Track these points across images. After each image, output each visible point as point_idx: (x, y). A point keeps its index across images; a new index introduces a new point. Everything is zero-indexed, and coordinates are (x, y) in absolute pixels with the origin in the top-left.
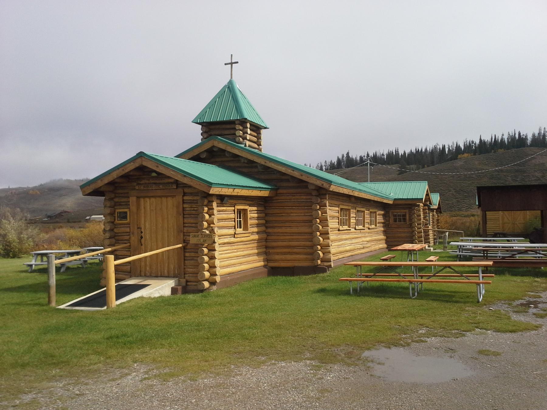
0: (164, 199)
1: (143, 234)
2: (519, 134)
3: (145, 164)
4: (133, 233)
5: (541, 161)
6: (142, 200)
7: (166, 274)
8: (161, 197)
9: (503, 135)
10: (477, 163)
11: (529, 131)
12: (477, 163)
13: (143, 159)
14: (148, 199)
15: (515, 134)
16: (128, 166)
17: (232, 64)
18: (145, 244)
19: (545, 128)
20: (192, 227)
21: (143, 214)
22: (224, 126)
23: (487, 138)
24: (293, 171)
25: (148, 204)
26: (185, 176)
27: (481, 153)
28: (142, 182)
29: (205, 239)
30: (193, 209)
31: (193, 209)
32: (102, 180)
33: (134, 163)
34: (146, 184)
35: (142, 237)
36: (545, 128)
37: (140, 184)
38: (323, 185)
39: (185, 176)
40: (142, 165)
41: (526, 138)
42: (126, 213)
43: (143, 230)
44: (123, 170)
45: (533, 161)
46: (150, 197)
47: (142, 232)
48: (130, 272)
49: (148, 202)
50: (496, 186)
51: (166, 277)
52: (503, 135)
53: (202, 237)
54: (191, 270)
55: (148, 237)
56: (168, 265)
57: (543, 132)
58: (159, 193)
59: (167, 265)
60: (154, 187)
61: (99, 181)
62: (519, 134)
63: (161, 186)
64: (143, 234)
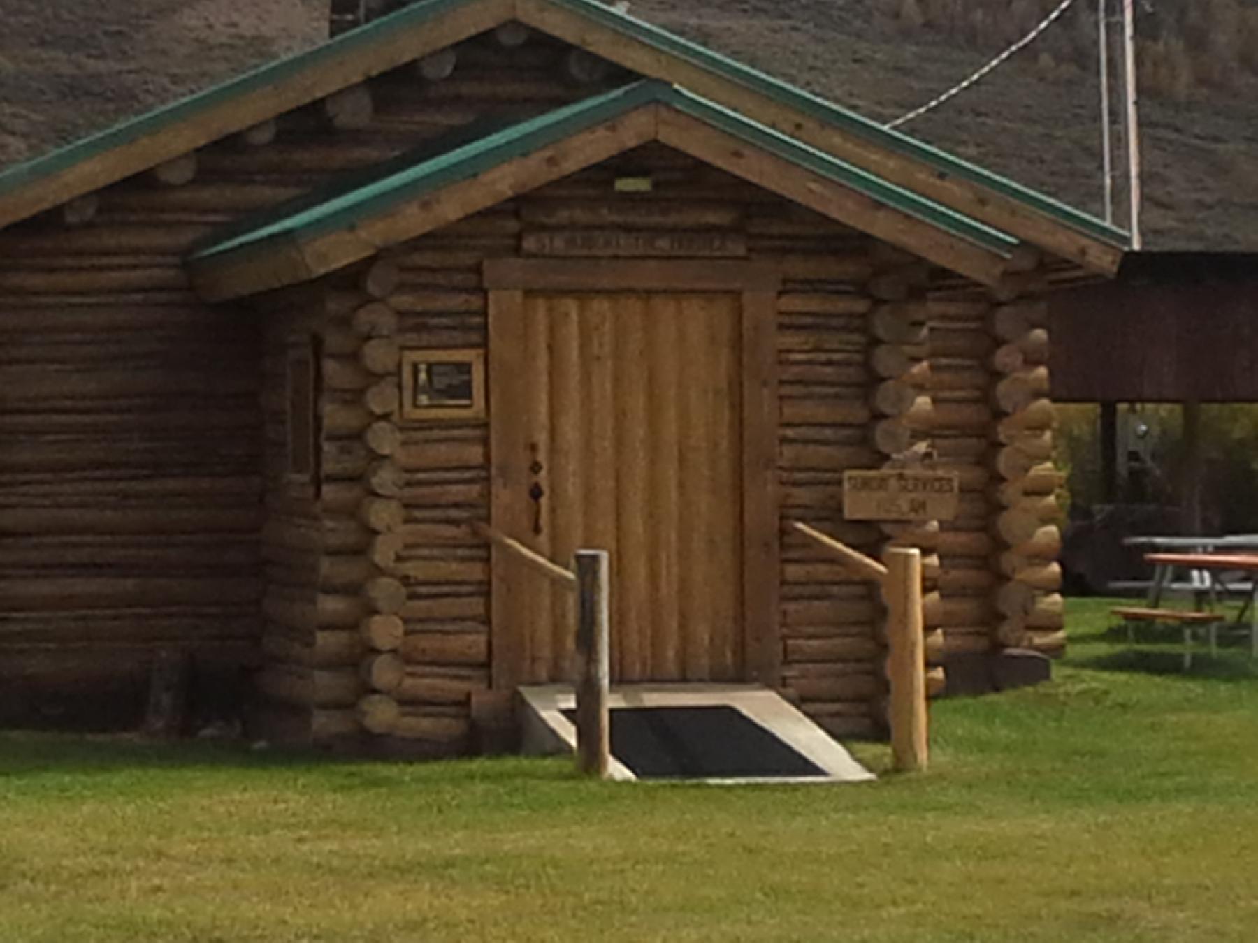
0: (666, 309)
1: (543, 477)
3: (671, 136)
4: (503, 471)
5: (247, 26)
6: (541, 305)
7: (672, 668)
13: (664, 113)
14: (571, 306)
16: (577, 141)
18: (553, 526)
20: (825, 443)
21: (544, 379)
24: (942, 176)
25: (573, 329)
26: (880, 206)
28: (552, 221)
29: (918, 496)
30: (823, 357)
31: (823, 357)
32: (425, 206)
33: (613, 128)
34: (572, 226)
35: (536, 493)
37: (543, 228)
38: (1083, 252)
39: (880, 206)
40: (656, 141)
42: (465, 368)
43: (542, 457)
46: (583, 294)
48: (487, 665)
49: (574, 316)
50: (1171, 255)
51: (672, 681)
53: (904, 489)
54: (814, 643)
55: (572, 489)
56: (682, 626)
58: (650, 275)
59: (674, 624)
60: (625, 245)
61: (413, 210)
63: (663, 244)
64: (543, 477)
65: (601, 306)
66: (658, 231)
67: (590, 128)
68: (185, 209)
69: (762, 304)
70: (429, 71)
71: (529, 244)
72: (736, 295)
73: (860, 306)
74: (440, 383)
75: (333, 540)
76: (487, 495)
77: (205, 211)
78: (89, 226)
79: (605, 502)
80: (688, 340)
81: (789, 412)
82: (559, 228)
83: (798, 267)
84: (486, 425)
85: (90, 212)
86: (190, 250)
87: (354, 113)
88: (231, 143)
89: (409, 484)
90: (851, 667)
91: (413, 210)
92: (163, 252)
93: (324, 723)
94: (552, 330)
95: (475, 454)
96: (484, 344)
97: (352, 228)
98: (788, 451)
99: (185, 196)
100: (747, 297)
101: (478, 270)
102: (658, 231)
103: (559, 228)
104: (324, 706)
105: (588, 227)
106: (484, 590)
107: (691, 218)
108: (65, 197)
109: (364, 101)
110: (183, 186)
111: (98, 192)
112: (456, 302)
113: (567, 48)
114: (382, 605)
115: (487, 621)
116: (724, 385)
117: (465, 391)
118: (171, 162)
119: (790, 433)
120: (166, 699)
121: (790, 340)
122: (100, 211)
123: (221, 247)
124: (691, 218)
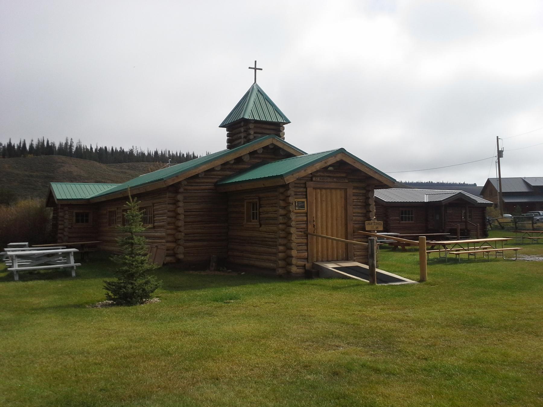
2: (48, 141)
5: (69, 170)
8: (331, 189)
9: (32, 141)
10: (6, 166)
11: (57, 140)
12: (6, 166)
15: (44, 141)
16: (330, 159)
17: (255, 69)
19: (72, 139)
22: (264, 126)
23: (16, 142)
25: (319, 196)
27: (10, 156)
32: (305, 171)
34: (320, 176)
36: (72, 139)
41: (14, 146)
42: (303, 202)
44: (326, 163)
45: (62, 169)
46: (321, 189)
47: (314, 221)
52: (32, 141)
54: (359, 253)
55: (319, 225)
57: (69, 144)
58: (333, 185)
60: (329, 180)
62: (48, 141)
63: (335, 180)
65: (324, 191)
66: (334, 177)
67: (332, 157)
68: (215, 175)
69: (350, 191)
70: (258, 152)
71: (314, 179)
72: (346, 189)
73: (364, 192)
74: (300, 205)
75: (281, 235)
76: (307, 226)
77: (218, 176)
78: (203, 178)
79: (325, 227)
80: (337, 197)
81: (354, 210)
82: (318, 176)
83: (356, 184)
84: (307, 213)
85: (203, 175)
86: (217, 182)
87: (247, 159)
88: (227, 163)
89: (297, 224)
90: (361, 257)
91: (303, 171)
92: (211, 183)
93: (280, 271)
94: (316, 195)
95: (305, 219)
96: (306, 198)
97: (293, 175)
98: (354, 218)
99: (219, 173)
100: (348, 190)
101: (305, 183)
102: (334, 177)
103: (318, 176)
104: (280, 268)
105: (323, 176)
106: (307, 244)
107: (338, 175)
108: (200, 172)
109: (248, 156)
110: (218, 171)
111: (205, 171)
112: (302, 190)
113: (280, 148)
114: (293, 248)
115: (307, 250)
116: (343, 206)
117: (303, 207)
118: (217, 166)
119: (354, 214)
120: (214, 264)
121: (354, 198)
122: (205, 175)
123: (230, 181)
124: (338, 175)
